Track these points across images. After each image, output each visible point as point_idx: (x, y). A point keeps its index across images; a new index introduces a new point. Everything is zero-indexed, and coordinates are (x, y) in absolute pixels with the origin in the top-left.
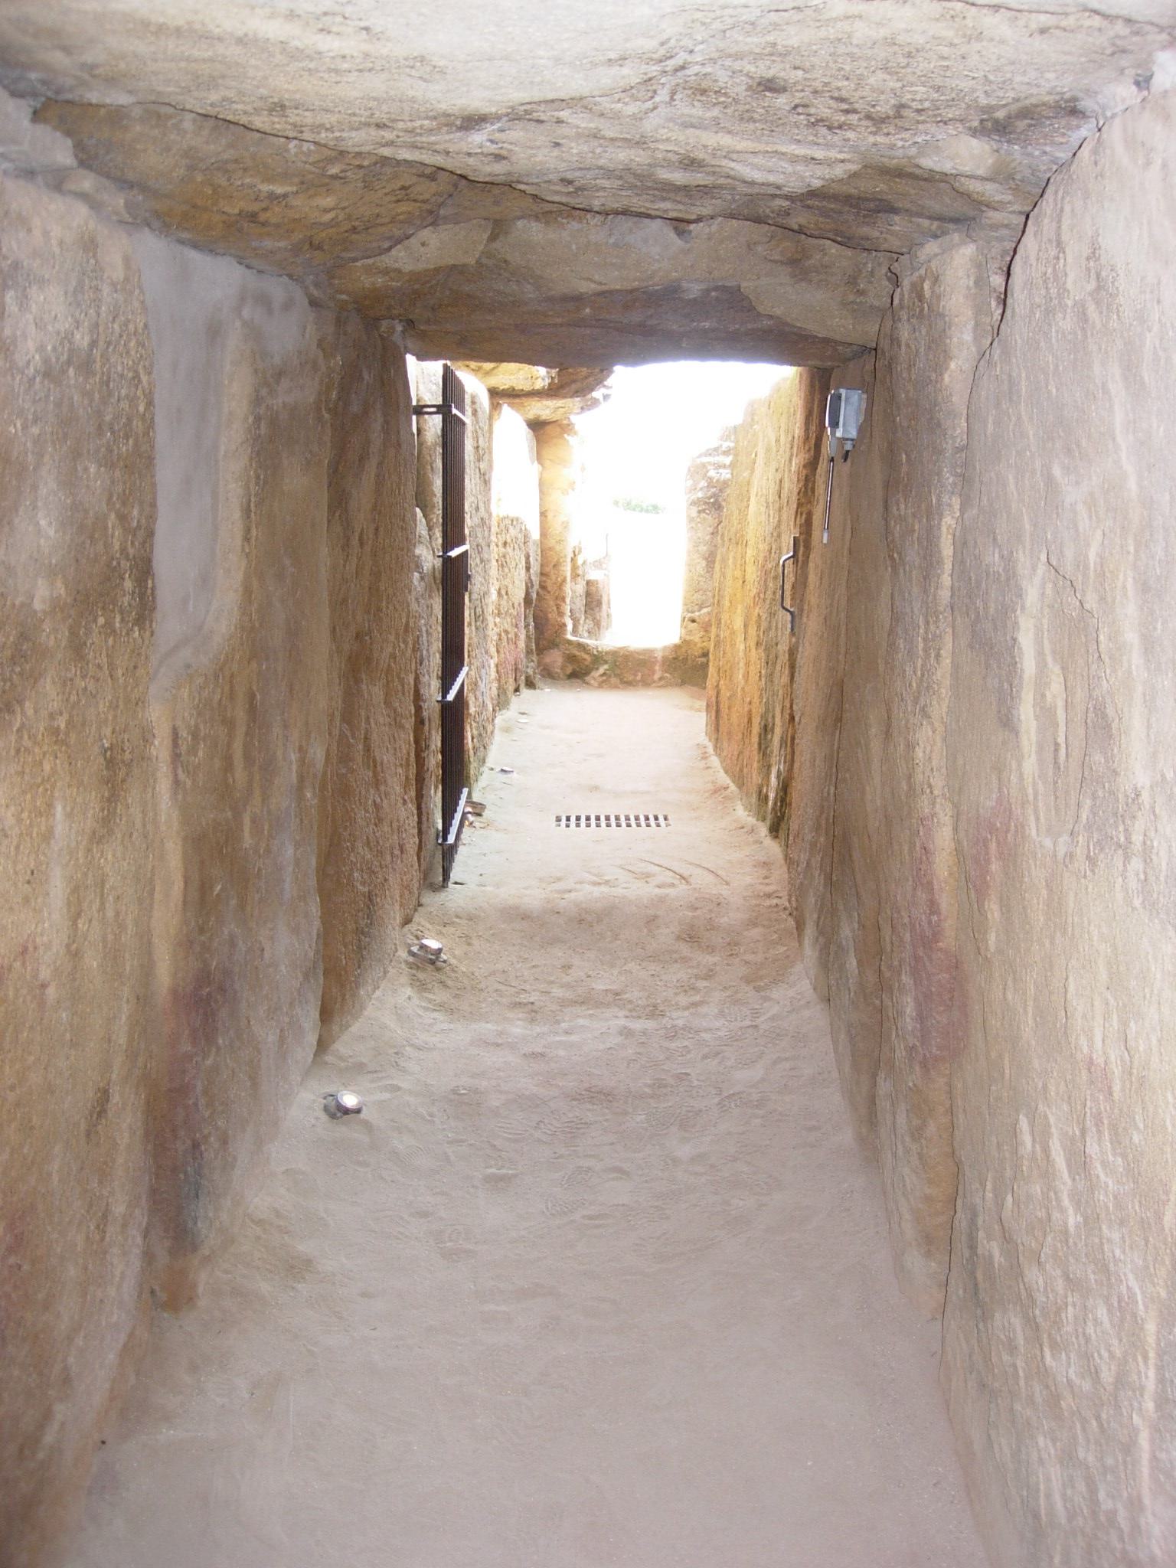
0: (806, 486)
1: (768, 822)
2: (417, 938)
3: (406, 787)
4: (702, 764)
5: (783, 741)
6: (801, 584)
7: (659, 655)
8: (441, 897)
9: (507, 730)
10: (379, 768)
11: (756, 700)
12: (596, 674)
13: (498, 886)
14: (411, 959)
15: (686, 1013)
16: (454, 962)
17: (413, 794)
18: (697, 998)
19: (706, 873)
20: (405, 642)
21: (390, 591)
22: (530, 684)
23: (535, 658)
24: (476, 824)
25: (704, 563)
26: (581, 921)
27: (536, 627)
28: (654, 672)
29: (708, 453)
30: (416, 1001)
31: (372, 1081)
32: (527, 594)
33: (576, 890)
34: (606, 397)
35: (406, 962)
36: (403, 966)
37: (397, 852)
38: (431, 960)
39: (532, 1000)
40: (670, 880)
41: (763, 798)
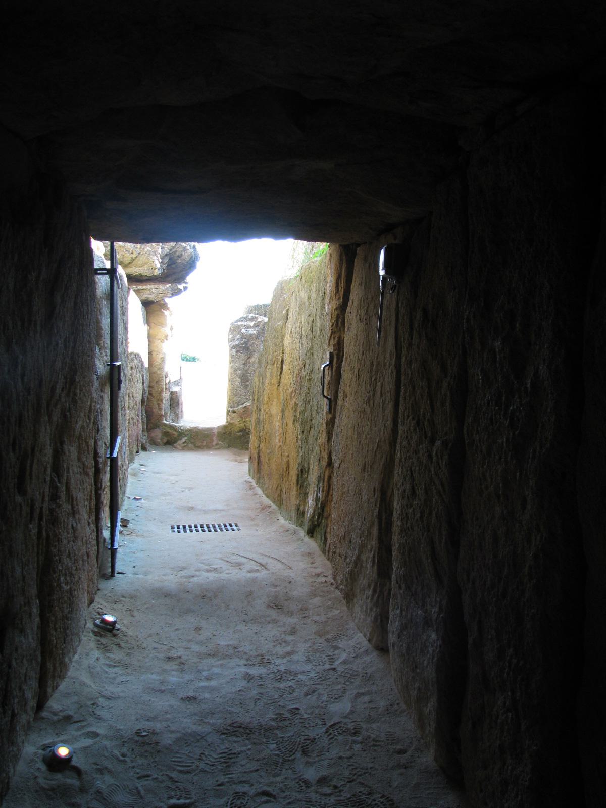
0: (337, 321)
1: (306, 527)
2: (99, 613)
3: (90, 513)
4: (251, 492)
5: (320, 479)
6: (337, 378)
7: (215, 431)
8: (111, 583)
9: (134, 475)
10: (75, 503)
11: (294, 454)
12: (180, 442)
13: (146, 574)
14: (96, 629)
15: (285, 660)
16: (124, 629)
17: (94, 518)
18: (289, 649)
19: (276, 562)
20: (89, 419)
21: (82, 383)
22: (144, 449)
23: (146, 434)
24: (125, 532)
25: (239, 380)
26: (203, 597)
27: (147, 417)
28: (213, 441)
29: (242, 319)
30: (102, 661)
31: (78, 729)
32: (143, 397)
33: (197, 576)
34: (185, 288)
35: (92, 631)
36: (91, 635)
37: (86, 558)
38: (108, 629)
39: (179, 654)
40: (255, 567)
41: (301, 513)
